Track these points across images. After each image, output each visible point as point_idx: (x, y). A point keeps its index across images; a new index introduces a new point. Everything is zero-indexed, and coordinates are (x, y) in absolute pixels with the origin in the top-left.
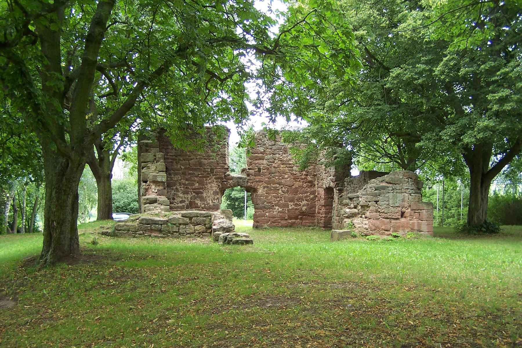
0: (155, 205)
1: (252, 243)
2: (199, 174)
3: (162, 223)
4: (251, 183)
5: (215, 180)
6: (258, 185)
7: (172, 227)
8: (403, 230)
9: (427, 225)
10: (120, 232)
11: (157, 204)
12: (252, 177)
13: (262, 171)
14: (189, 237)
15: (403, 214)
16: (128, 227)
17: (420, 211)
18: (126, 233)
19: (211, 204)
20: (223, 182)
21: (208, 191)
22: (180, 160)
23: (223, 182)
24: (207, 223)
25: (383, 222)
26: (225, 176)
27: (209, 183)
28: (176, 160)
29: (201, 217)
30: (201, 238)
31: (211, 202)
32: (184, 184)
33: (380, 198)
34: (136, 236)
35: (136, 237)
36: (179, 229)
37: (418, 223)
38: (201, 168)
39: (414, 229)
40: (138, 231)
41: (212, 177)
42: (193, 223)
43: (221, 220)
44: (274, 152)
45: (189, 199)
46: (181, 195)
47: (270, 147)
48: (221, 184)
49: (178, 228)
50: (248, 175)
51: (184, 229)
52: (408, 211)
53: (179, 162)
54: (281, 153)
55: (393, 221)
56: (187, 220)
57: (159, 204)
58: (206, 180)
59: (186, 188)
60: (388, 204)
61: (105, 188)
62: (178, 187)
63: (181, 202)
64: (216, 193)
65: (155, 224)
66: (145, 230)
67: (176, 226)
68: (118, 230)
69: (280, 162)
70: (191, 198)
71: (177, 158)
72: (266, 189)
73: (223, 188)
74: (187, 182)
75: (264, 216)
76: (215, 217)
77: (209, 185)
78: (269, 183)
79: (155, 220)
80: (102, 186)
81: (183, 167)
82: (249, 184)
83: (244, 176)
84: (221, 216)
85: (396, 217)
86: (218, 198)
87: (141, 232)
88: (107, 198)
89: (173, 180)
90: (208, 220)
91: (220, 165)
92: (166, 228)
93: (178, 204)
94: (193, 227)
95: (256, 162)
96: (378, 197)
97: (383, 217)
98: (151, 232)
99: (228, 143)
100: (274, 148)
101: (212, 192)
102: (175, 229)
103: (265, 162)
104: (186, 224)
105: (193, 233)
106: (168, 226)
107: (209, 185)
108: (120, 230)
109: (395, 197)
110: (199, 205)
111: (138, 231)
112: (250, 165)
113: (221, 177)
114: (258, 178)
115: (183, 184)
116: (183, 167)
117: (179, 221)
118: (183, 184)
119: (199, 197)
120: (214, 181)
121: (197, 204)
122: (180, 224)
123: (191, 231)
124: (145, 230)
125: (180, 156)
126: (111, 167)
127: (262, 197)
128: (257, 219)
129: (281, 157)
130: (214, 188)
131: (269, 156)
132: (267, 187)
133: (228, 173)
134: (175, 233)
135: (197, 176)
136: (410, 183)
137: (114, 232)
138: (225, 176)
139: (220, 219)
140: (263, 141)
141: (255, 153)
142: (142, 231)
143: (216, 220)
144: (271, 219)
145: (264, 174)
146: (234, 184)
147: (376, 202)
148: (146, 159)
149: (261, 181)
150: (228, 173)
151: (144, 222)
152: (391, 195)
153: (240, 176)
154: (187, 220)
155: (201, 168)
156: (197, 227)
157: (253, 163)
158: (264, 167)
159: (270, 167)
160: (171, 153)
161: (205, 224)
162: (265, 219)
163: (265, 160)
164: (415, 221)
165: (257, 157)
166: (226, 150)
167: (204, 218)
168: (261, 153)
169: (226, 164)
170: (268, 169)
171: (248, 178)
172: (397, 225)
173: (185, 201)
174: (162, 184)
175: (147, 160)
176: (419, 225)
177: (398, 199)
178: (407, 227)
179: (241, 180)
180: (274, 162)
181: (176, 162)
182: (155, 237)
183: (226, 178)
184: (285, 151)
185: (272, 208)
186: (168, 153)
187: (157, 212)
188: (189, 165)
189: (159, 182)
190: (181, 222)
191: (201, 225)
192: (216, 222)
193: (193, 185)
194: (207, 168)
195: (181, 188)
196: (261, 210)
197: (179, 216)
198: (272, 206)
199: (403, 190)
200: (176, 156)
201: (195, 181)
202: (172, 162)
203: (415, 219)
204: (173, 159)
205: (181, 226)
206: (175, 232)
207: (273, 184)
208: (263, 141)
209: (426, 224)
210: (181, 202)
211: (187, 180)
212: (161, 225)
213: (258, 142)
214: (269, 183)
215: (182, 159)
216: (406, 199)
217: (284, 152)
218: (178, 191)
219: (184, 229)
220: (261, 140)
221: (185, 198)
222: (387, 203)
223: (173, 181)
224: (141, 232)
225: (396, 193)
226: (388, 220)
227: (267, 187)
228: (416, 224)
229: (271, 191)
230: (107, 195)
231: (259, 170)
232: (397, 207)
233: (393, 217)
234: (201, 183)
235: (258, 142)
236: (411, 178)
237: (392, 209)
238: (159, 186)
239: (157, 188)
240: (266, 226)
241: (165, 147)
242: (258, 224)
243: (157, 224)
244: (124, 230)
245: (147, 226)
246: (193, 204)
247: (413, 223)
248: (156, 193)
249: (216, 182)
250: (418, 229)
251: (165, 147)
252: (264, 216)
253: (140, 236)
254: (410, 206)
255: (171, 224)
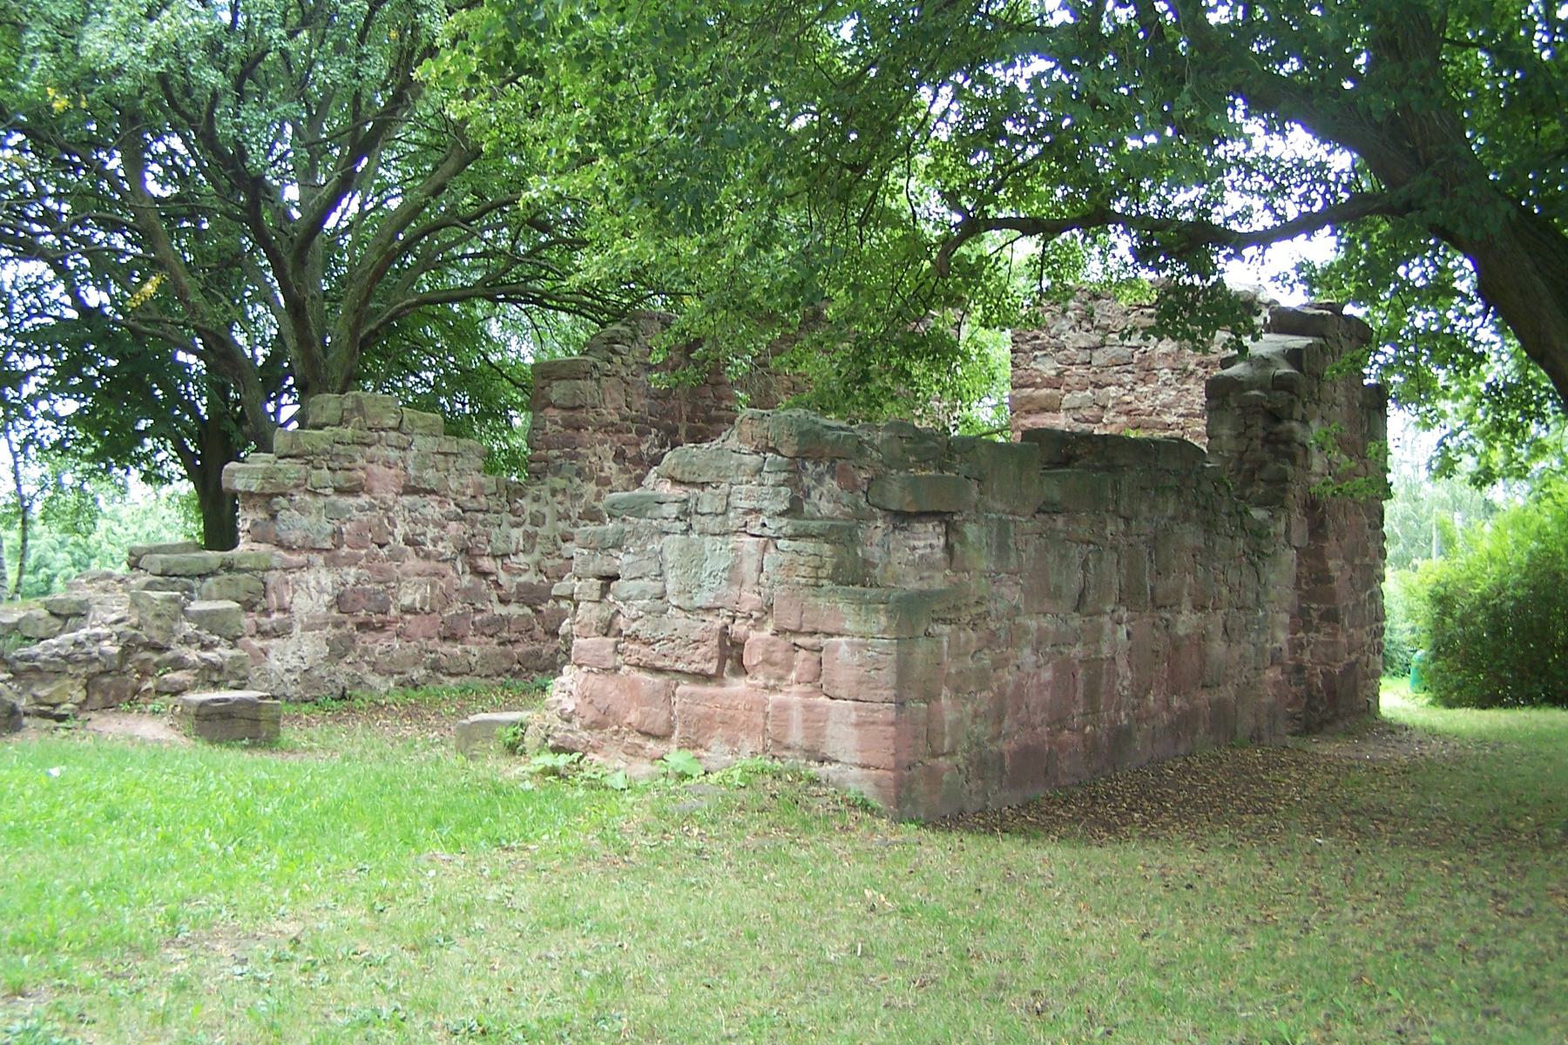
8: (728, 741)
9: (857, 725)
15: (731, 653)
17: (825, 641)
25: (634, 686)
33: (622, 561)
37: (808, 708)
39: (789, 741)
44: (1099, 377)
47: (1083, 356)
52: (758, 640)
54: (1128, 378)
55: (685, 687)
60: (658, 591)
69: (1124, 418)
85: (693, 667)
96: (614, 552)
97: (634, 660)
100: (1099, 357)
109: (693, 559)
129: (1127, 398)
131: (1080, 395)
136: (770, 480)
140: (1053, 331)
147: (609, 579)
152: (672, 545)
163: (1062, 414)
164: (793, 695)
165: (1030, 399)
168: (1048, 383)
172: (701, 710)
174: (261, 502)
176: (813, 720)
177: (708, 566)
178: (750, 729)
180: (1099, 420)
184: (1148, 373)
199: (734, 520)
203: (796, 688)
208: (1053, 331)
209: (853, 717)
216: (749, 567)
217: (1142, 374)
222: (657, 586)
225: (701, 533)
226: (659, 680)
228: (796, 716)
232: (708, 610)
233: (679, 666)
235: (1037, 338)
236: (774, 450)
237: (680, 621)
247: (783, 708)
250: (806, 744)
254: (768, 609)
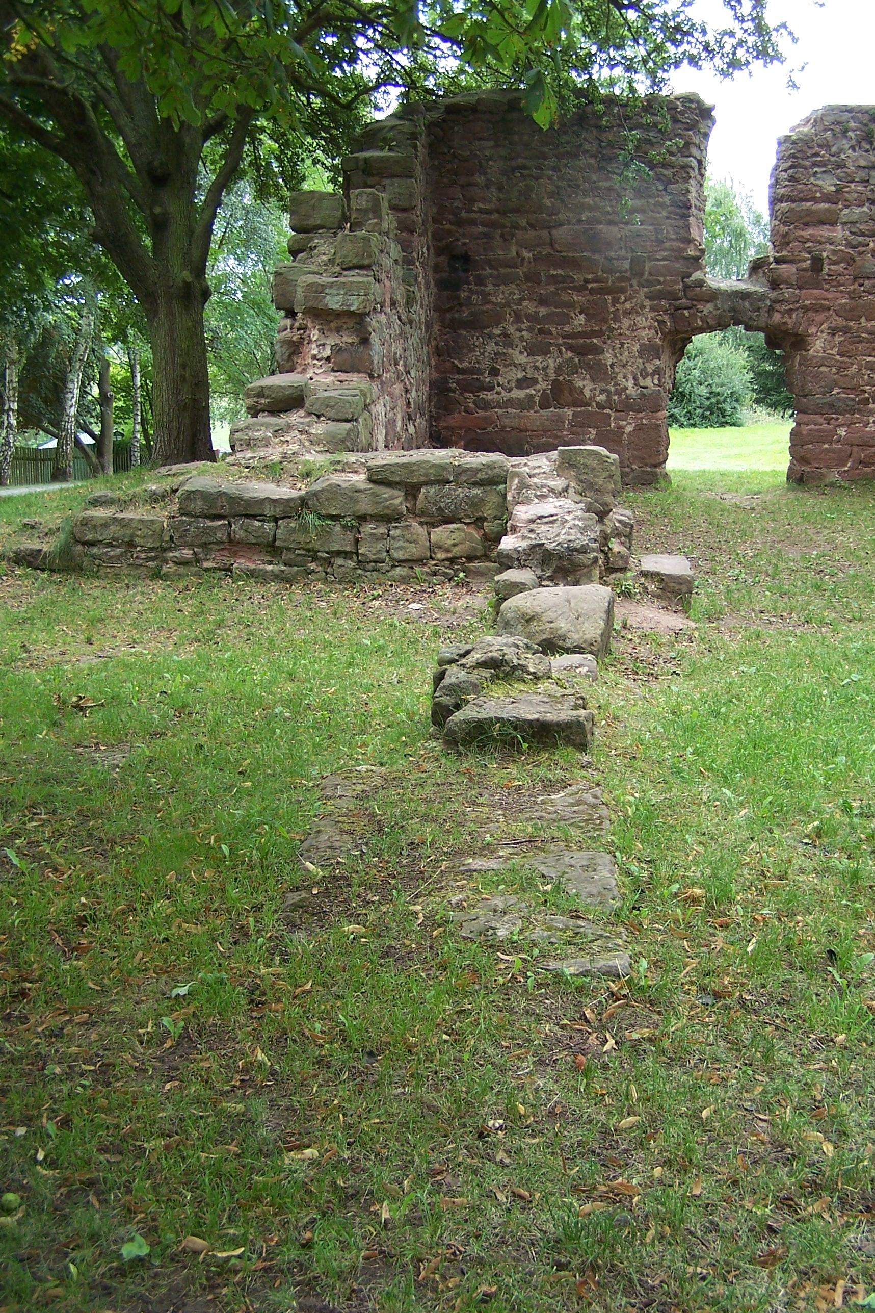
0: (295, 417)
1: (583, 747)
2: (587, 281)
3: (278, 511)
4: (783, 314)
5: (647, 303)
6: (811, 322)
7: (325, 533)
10: (95, 550)
11: (302, 413)
12: (787, 292)
13: (826, 267)
14: (404, 580)
16: (129, 532)
18: (118, 558)
19: (632, 390)
20: (677, 309)
21: (622, 344)
22: (516, 227)
23: (677, 309)
24: (488, 512)
26: (686, 287)
27: (627, 313)
28: (503, 226)
29: (459, 485)
30: (460, 585)
31: (630, 383)
32: (533, 318)
34: (165, 569)
35: (165, 577)
36: (357, 541)
38: (597, 257)
40: (172, 544)
41: (636, 292)
42: (423, 513)
43: (550, 507)
45: (551, 371)
46: (522, 359)
47: (862, 174)
48: (672, 316)
49: (350, 537)
50: (774, 284)
51: (381, 538)
53: (513, 235)
56: (396, 499)
57: (310, 414)
58: (615, 301)
59: (541, 331)
61: (173, 339)
62: (511, 330)
63: (522, 383)
64: (649, 351)
65: (247, 516)
66: (205, 545)
67: (344, 527)
68: (84, 543)
70: (558, 370)
71: (506, 221)
72: (838, 339)
73: (677, 332)
74: (543, 311)
75: (828, 437)
76: (523, 486)
77: (626, 323)
78: (851, 314)
79: (247, 495)
80: (162, 332)
81: (527, 255)
82: (777, 317)
83: (758, 287)
84: (552, 483)
86: (657, 371)
87: (187, 553)
88: (183, 377)
89: (490, 302)
90: (494, 499)
91: (667, 245)
92: (294, 537)
93: (510, 390)
94: (421, 531)
95: (807, 233)
98: (234, 554)
99: (700, 162)
101: (636, 348)
102: (340, 540)
103: (839, 233)
104: (390, 518)
105: (421, 561)
106: (304, 528)
107: (626, 323)
108: (92, 544)
110: (587, 393)
111: (170, 549)
112: (781, 244)
113: (669, 292)
114: (809, 296)
115: (529, 318)
116: (527, 255)
117: (357, 501)
118: (529, 318)
119: (589, 367)
120: (643, 307)
121: (582, 392)
122: (362, 518)
123: (414, 551)
124: (205, 545)
125: (517, 210)
126: (196, 253)
127: (822, 369)
128: (802, 452)
130: (645, 334)
131: (857, 210)
132: (846, 330)
133: (697, 275)
134: (339, 561)
135: (581, 289)
137: (65, 552)
138: (686, 287)
139: (542, 497)
140: (834, 149)
141: (802, 200)
142: (191, 546)
143: (527, 501)
144: (855, 449)
145: (834, 281)
146: (720, 317)
148: (308, 216)
149: (822, 306)
150: (697, 275)
151: (198, 506)
153: (742, 286)
154: (396, 499)
155: (597, 257)
156: (441, 534)
157: (796, 239)
158: (834, 252)
159: (860, 253)
160: (483, 200)
161: (481, 519)
162: (833, 451)
165: (809, 212)
166: (693, 190)
167: (476, 491)
168: (827, 198)
169: (689, 241)
170: (850, 261)
171: (773, 295)
173: (535, 381)
175: (311, 222)
179: (747, 304)
181: (502, 236)
182: (252, 574)
183: (690, 294)
185: (860, 411)
186: (472, 201)
187: (274, 454)
188: (552, 245)
189: (337, 314)
190: (365, 506)
191: (460, 521)
192: (522, 513)
193: (567, 320)
194: (618, 259)
195: (522, 333)
196: (819, 419)
197: (359, 479)
198: (859, 403)
200: (503, 213)
201: (571, 305)
202: (486, 235)
204: (492, 225)
205: (368, 528)
206: (338, 553)
207: (868, 320)
208: (834, 149)
210: (522, 383)
211: (542, 302)
212: (276, 520)
213: (817, 155)
214: (851, 314)
215: (523, 223)
218: (511, 345)
219: (381, 538)
220: (826, 146)
221: (536, 368)
223: (489, 307)
224: (187, 553)
227: (846, 330)
229: (860, 346)
230: (184, 366)
231: (817, 263)
234: (594, 313)
235: (817, 155)
238: (338, 330)
239: (331, 341)
240: (834, 476)
241: (462, 180)
242: (807, 469)
243: (254, 517)
244: (110, 545)
245: (209, 523)
246: (566, 393)
248: (328, 359)
249: (653, 309)
251: (462, 180)
252: (828, 437)
253: (182, 570)
255: (321, 517)
